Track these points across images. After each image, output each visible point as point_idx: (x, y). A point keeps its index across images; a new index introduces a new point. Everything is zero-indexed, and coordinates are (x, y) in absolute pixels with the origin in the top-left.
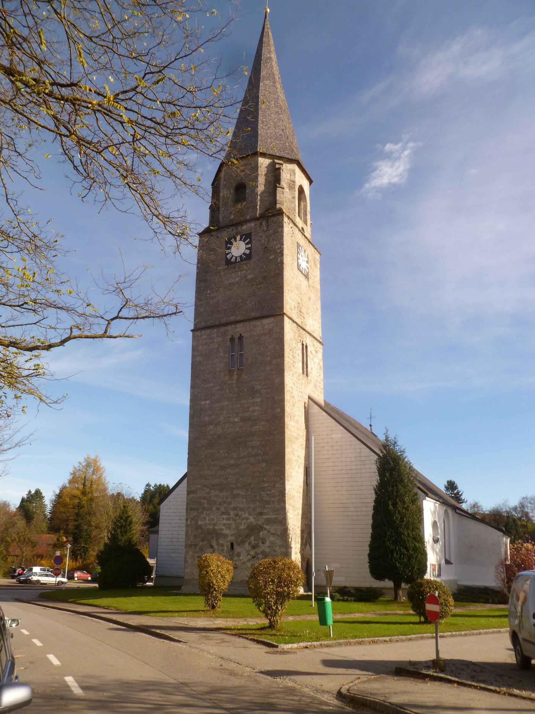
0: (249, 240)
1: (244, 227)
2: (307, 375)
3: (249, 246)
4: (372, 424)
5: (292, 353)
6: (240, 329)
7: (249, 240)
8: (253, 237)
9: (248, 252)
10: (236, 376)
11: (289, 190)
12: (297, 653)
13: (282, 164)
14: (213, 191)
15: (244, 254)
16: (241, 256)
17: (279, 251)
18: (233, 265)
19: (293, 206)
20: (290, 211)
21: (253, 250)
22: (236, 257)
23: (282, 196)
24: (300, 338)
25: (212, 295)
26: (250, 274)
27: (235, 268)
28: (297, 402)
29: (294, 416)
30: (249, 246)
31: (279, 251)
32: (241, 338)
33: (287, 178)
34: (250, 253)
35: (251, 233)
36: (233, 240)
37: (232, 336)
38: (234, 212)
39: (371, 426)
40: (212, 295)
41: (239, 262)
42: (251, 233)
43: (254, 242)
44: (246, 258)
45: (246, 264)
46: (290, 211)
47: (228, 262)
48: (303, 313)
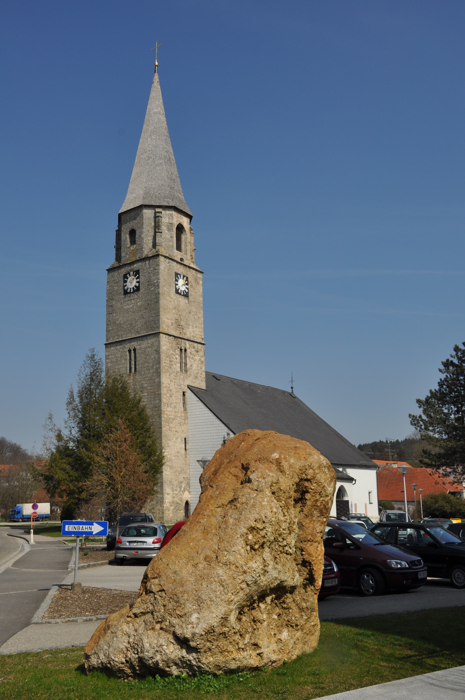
0: (138, 275)
1: (135, 265)
2: (186, 371)
3: (138, 280)
4: (293, 386)
5: (169, 359)
6: (134, 344)
7: (138, 275)
8: (140, 274)
9: (137, 285)
10: (132, 377)
11: (168, 231)
12: (8, 535)
13: (161, 212)
14: (116, 234)
15: (135, 286)
16: (133, 288)
17: (156, 284)
18: (129, 295)
19: (171, 244)
20: (169, 248)
21: (140, 283)
22: (131, 289)
23: (160, 239)
24: (178, 346)
25: (116, 318)
26: (139, 302)
27: (130, 297)
28: (175, 393)
29: (171, 404)
30: (138, 280)
31: (156, 284)
32: (135, 350)
33: (166, 221)
34: (139, 285)
35: (139, 270)
36: (128, 275)
37: (129, 348)
38: (128, 253)
39: (292, 388)
40: (116, 318)
41: (132, 292)
42: (139, 270)
43: (141, 277)
44: (137, 289)
45: (137, 294)
46: (169, 248)
47: (126, 293)
48: (182, 326)
